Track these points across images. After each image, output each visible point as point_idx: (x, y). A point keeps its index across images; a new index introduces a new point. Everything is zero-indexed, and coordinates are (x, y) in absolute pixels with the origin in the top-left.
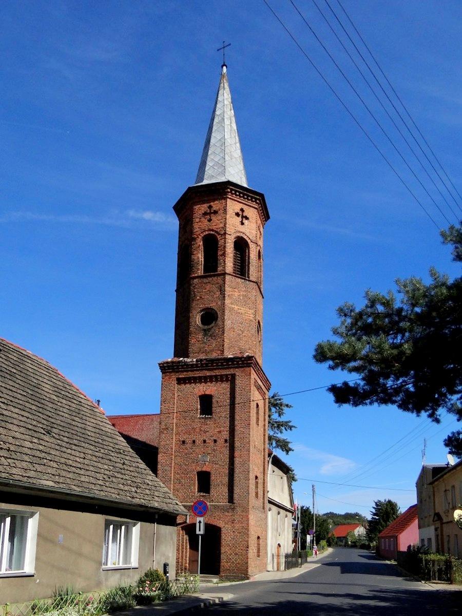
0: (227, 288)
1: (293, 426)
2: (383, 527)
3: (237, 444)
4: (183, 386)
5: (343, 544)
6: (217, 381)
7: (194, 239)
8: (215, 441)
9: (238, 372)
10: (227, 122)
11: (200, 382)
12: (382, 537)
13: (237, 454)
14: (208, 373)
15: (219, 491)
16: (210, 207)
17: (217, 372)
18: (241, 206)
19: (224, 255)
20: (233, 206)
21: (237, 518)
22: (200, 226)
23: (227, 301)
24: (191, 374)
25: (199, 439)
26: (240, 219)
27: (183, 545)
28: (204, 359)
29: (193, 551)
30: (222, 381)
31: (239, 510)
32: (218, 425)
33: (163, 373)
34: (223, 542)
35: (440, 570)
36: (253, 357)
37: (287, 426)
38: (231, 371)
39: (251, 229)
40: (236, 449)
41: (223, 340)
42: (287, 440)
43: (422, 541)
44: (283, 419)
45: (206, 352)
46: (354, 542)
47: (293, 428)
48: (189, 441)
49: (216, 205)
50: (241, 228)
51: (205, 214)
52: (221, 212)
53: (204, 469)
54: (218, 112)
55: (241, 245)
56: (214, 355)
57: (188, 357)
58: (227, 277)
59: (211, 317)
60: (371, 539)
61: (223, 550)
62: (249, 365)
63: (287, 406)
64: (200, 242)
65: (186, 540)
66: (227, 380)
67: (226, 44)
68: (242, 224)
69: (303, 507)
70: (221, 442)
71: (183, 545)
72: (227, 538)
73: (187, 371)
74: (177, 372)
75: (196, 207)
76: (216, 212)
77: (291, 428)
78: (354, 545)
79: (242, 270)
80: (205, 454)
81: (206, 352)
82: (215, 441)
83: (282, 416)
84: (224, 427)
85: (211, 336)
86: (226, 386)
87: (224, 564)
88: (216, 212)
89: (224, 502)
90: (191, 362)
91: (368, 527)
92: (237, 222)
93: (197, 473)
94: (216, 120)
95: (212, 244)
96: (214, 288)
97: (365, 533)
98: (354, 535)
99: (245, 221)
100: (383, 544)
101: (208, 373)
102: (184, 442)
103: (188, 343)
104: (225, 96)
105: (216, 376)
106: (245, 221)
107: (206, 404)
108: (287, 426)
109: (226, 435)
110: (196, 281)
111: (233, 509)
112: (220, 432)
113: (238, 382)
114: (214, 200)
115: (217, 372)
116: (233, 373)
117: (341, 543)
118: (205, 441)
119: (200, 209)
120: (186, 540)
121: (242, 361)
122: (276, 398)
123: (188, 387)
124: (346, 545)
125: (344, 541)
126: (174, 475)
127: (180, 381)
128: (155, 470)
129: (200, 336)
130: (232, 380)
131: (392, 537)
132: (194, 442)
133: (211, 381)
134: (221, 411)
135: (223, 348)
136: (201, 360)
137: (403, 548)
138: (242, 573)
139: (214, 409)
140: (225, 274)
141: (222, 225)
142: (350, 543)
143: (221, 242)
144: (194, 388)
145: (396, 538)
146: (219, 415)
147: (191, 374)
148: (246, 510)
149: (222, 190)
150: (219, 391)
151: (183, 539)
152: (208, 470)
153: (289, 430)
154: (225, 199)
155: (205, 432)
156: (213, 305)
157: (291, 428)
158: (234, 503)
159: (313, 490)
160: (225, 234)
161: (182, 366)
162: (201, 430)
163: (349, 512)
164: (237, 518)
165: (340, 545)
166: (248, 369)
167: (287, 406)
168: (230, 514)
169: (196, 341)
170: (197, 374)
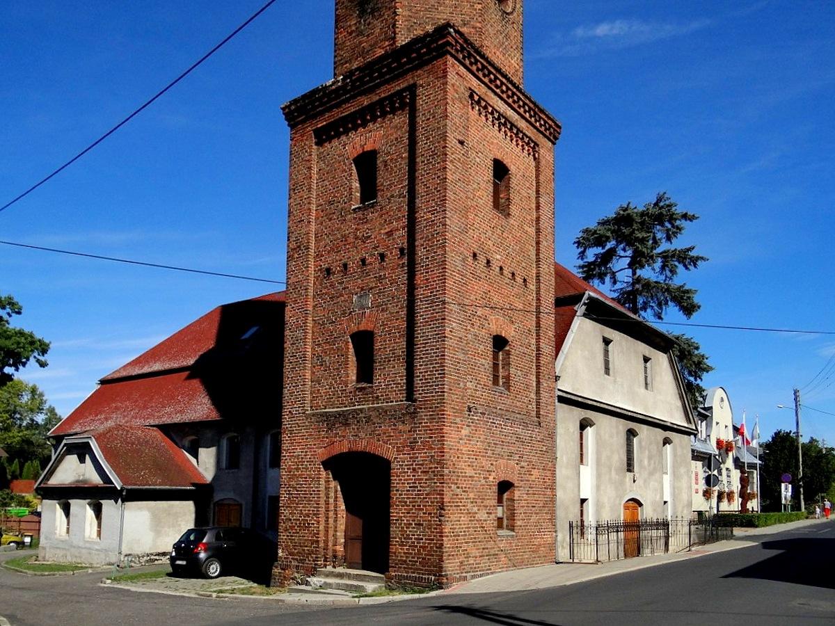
1: (698, 258)
3: (421, 252)
15: (389, 376)
17: (384, 92)
21: (421, 436)
25: (354, 257)
27: (327, 503)
28: (356, 69)
29: (353, 517)
31: (424, 415)
33: (292, 126)
34: (395, 496)
36: (448, 25)
37: (686, 258)
40: (418, 267)
41: (395, 12)
42: (686, 288)
44: (678, 244)
47: (699, 263)
48: (337, 268)
53: (362, 328)
61: (395, 513)
62: (442, 52)
63: (685, 216)
65: (336, 491)
70: (393, 256)
71: (327, 503)
72: (402, 484)
73: (329, 109)
74: (314, 117)
77: (694, 261)
80: (364, 292)
81: (363, 53)
82: (382, 256)
83: (674, 240)
84: (398, 219)
85: (372, 13)
87: (398, 550)
89: (397, 398)
90: (334, 83)
93: (351, 336)
101: (365, 101)
102: (328, 271)
108: (686, 258)
111: (413, 415)
112: (390, 234)
115: (384, 92)
116: (412, 82)
118: (363, 261)
120: (336, 491)
121: (427, 46)
122: (662, 204)
123: (334, 146)
126: (313, 349)
132: (345, 266)
134: (392, 181)
135: (395, 33)
138: (430, 571)
144: (344, 146)
146: (389, 194)
148: (438, 415)
151: (327, 489)
152: (370, 327)
153: (691, 267)
157: (694, 261)
158: (415, 401)
159: (795, 399)
161: (320, 99)
162: (357, 238)
164: (421, 436)
166: (441, 61)
167: (685, 216)
168: (408, 427)
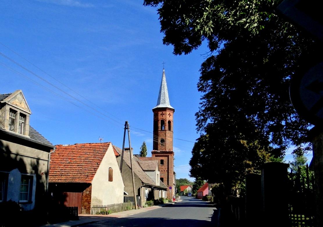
0: (167, 134)
2: (198, 187)
4: (157, 157)
5: (182, 194)
6: (165, 157)
7: (159, 121)
8: (164, 171)
9: (169, 155)
10: (165, 87)
11: (161, 157)
12: (199, 192)
13: (169, 174)
14: (163, 155)
16: (162, 113)
18: (170, 112)
19: (166, 125)
20: (168, 112)
22: (160, 117)
23: (167, 137)
24: (159, 155)
26: (169, 116)
30: (166, 157)
32: (165, 167)
35: (210, 199)
38: (168, 155)
39: (171, 118)
43: (209, 193)
45: (162, 150)
46: (186, 194)
49: (164, 112)
50: (170, 118)
51: (161, 114)
52: (165, 114)
54: (163, 84)
55: (169, 122)
56: (164, 151)
57: (157, 150)
58: (167, 131)
59: (163, 141)
60: (194, 193)
62: (172, 153)
64: (160, 122)
66: (167, 157)
67: (164, 63)
68: (170, 117)
69: (9, 124)
70: (166, 171)
75: (159, 112)
76: (164, 114)
78: (187, 195)
79: (170, 129)
86: (167, 158)
88: (164, 114)
91: (192, 187)
92: (168, 117)
94: (163, 86)
95: (163, 122)
96: (164, 134)
97: (191, 190)
98: (187, 190)
99: (170, 116)
100: (198, 194)
101: (163, 155)
103: (158, 147)
104: (164, 79)
105: (164, 155)
106: (170, 116)
107: (162, 162)
109: (167, 169)
110: (159, 131)
113: (169, 157)
114: (163, 111)
117: (181, 194)
119: (160, 113)
124: (183, 195)
125: (182, 193)
127: (156, 156)
128: (163, 182)
129: (161, 145)
130: (168, 156)
131: (201, 192)
133: (163, 157)
136: (161, 151)
137: (204, 195)
139: (164, 163)
140: (166, 130)
141: (165, 118)
142: (185, 194)
143: (165, 122)
145: (202, 192)
147: (159, 155)
149: (165, 109)
150: (165, 159)
152: (163, 177)
154: (166, 111)
155: (162, 169)
156: (163, 138)
160: (166, 120)
163: (182, 178)
165: (181, 195)
169: (160, 146)
170: (160, 155)
